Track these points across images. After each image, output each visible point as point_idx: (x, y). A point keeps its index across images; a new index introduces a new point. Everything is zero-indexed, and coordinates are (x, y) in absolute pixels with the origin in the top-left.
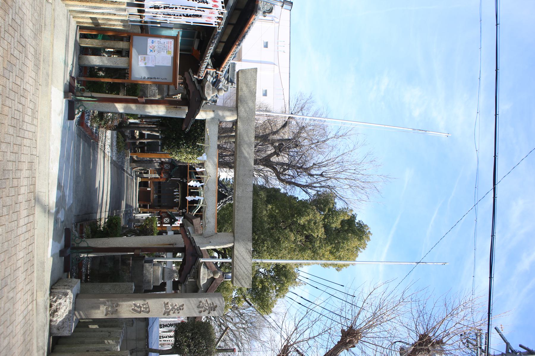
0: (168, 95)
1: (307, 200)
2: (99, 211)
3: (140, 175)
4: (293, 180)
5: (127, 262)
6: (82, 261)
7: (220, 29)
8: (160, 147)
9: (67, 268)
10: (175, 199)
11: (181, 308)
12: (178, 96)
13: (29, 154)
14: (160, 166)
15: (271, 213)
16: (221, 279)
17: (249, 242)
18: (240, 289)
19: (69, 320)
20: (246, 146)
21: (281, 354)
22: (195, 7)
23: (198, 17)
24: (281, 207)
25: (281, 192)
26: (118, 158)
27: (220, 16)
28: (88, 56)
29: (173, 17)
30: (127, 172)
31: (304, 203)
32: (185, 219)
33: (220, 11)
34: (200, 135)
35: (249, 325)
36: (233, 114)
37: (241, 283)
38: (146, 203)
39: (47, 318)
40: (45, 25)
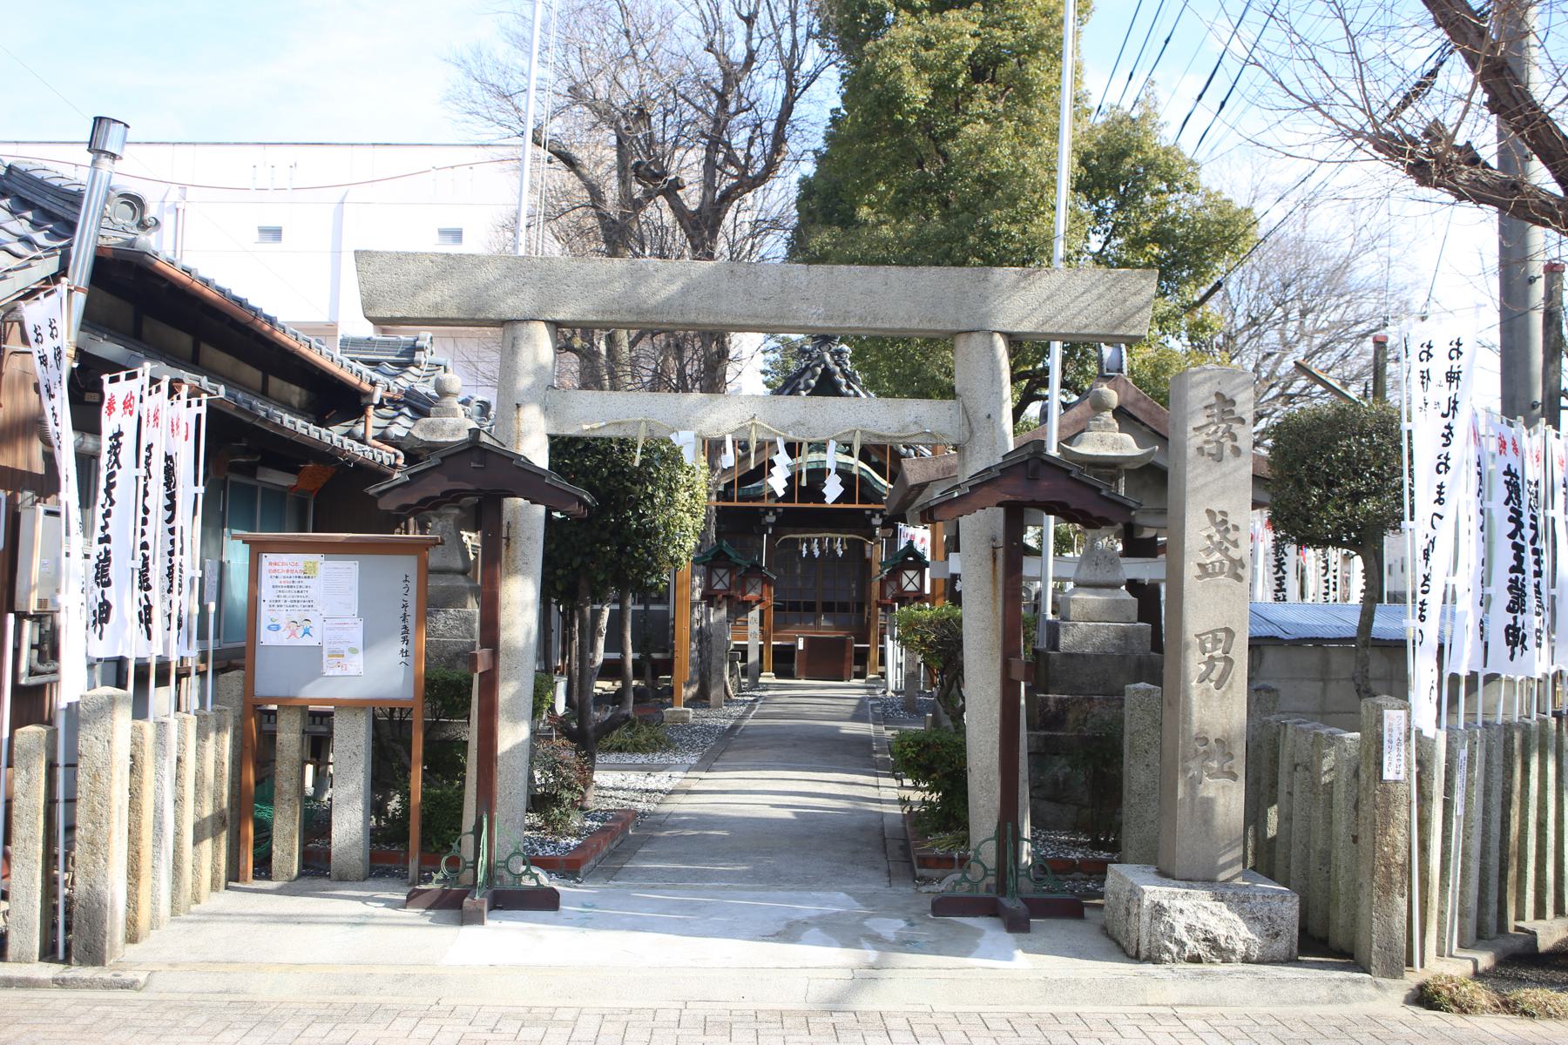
0: (464, 573)
1: (843, 76)
2: (874, 807)
3: (751, 672)
4: (770, 127)
5: (1053, 709)
6: (1047, 861)
7: (217, 390)
8: (652, 607)
9: (1072, 910)
10: (835, 552)
11: (1219, 518)
12: (469, 543)
13: (678, 1032)
14: (720, 602)
15: (891, 212)
16: (1123, 386)
17: (990, 277)
18: (1161, 321)
19: (1246, 899)
20: (642, 290)
21: (1403, 163)
22: (137, 478)
23: (172, 468)
24: (866, 171)
25: (811, 175)
26: (692, 748)
27: (165, 386)
28: (333, 850)
29: (177, 559)
30: (742, 718)
31: (855, 87)
32: (908, 513)
33: (147, 389)
34: (605, 457)
35: (1292, 290)
36: (529, 337)
37: (1140, 309)
38: (847, 655)
39: (1237, 972)
40: (227, 992)
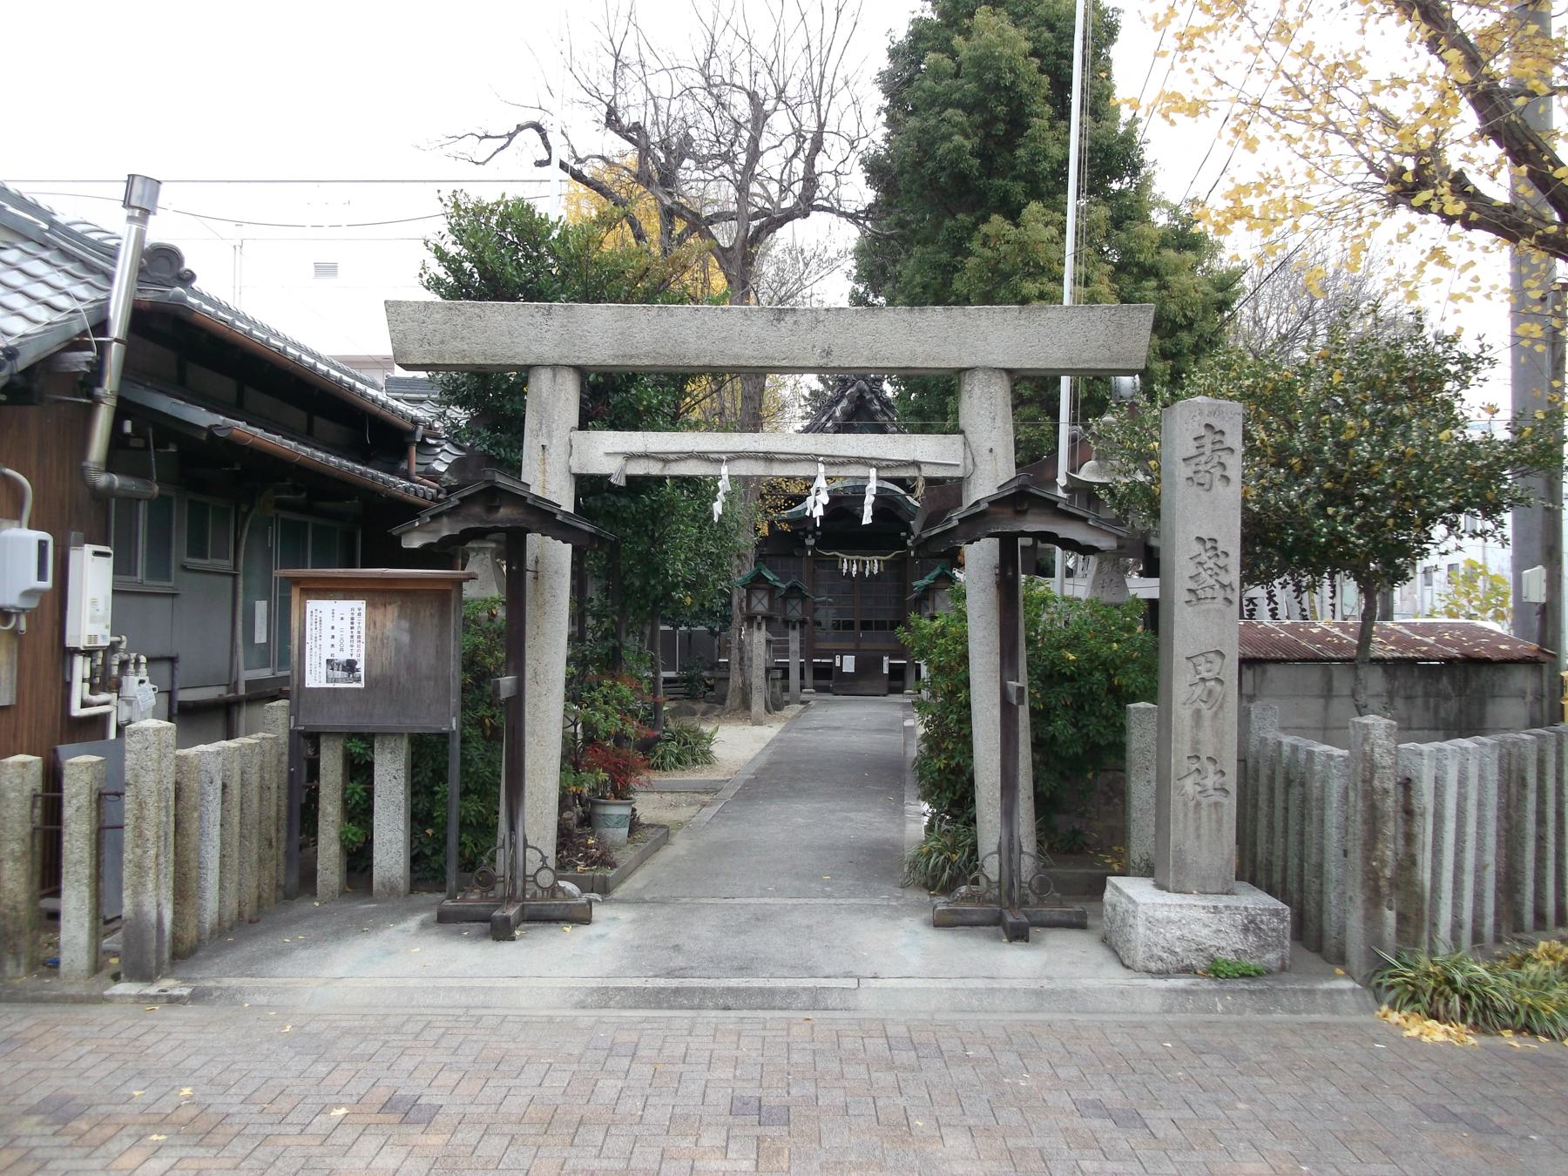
11: (1209, 545)
